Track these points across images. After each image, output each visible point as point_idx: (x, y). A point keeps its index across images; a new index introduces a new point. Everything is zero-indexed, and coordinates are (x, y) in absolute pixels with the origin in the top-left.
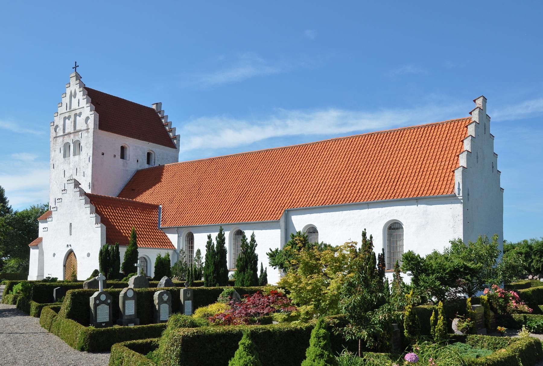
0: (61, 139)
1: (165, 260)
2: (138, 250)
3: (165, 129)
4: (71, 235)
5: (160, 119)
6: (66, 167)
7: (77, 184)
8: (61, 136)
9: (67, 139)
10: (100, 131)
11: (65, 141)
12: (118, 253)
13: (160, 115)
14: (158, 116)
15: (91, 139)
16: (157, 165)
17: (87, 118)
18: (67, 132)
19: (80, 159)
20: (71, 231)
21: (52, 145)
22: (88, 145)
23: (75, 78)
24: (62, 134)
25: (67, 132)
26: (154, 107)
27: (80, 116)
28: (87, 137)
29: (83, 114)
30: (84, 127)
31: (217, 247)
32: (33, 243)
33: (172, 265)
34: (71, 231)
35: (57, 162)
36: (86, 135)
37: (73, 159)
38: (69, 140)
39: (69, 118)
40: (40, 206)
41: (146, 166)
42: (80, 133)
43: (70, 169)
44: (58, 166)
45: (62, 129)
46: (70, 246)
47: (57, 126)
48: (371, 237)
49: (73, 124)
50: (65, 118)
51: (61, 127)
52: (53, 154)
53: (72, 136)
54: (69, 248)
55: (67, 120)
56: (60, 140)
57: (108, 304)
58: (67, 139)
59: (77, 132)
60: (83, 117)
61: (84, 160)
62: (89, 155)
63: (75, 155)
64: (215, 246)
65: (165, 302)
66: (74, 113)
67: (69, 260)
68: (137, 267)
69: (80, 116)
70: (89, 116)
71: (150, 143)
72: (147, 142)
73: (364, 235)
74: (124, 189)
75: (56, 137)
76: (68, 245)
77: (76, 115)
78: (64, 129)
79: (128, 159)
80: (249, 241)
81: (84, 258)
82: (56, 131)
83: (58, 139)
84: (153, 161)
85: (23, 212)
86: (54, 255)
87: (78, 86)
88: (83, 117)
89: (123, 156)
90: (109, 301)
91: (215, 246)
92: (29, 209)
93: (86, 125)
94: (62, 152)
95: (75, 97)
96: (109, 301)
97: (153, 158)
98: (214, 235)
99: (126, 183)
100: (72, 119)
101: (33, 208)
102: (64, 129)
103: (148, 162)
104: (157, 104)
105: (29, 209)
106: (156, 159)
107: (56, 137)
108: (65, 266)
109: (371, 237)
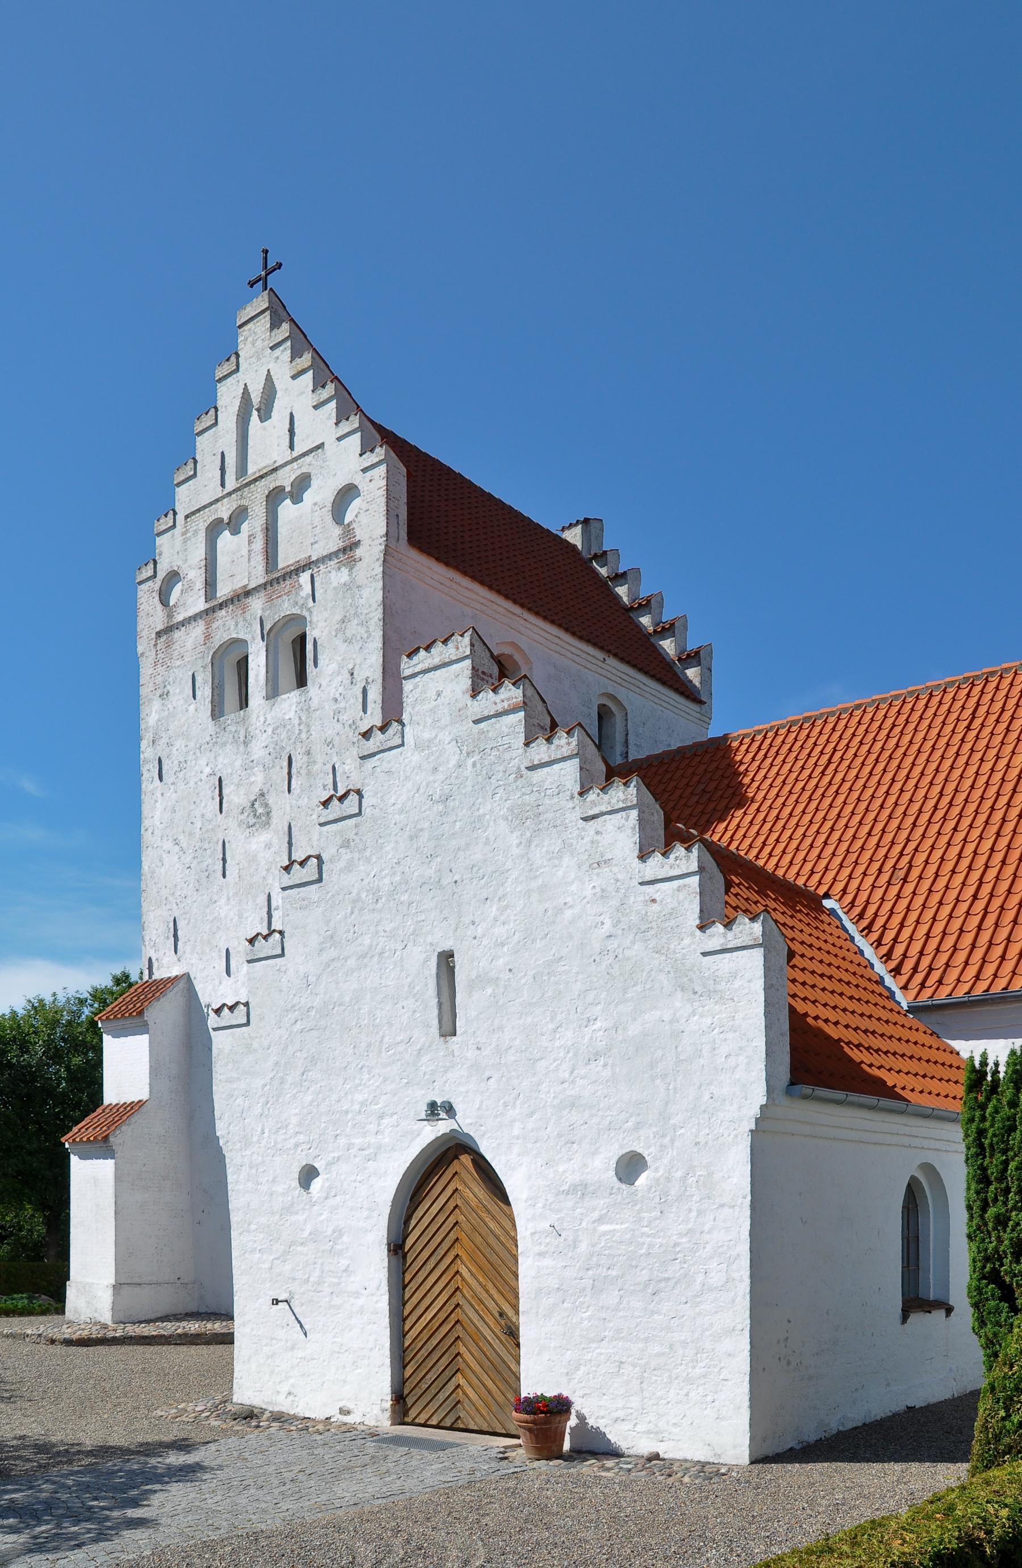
0: (198, 630)
3: (639, 627)
4: (448, 1029)
5: (604, 589)
6: (228, 761)
8: (194, 618)
9: (228, 626)
10: (414, 555)
11: (220, 637)
13: (603, 571)
14: (596, 574)
15: (372, 595)
17: (347, 493)
18: (224, 591)
19: (306, 708)
21: (146, 669)
22: (353, 628)
23: (265, 320)
24: (201, 605)
25: (224, 591)
26: (574, 537)
27: (297, 499)
28: (347, 587)
29: (315, 483)
30: (332, 539)
35: (179, 743)
37: (269, 714)
39: (235, 523)
40: (62, 999)
42: (305, 578)
43: (248, 767)
44: (182, 766)
45: (200, 584)
46: (450, 1110)
47: (174, 577)
49: (259, 544)
50: (214, 530)
51: (195, 575)
52: (152, 714)
53: (257, 605)
54: (443, 1127)
55: (225, 540)
56: (190, 638)
58: (228, 626)
59: (284, 577)
60: (320, 494)
61: (329, 708)
62: (360, 677)
63: (273, 692)
66: (262, 489)
67: (429, 1209)
69: (297, 499)
70: (359, 480)
71: (612, 661)
72: (600, 655)
75: (169, 630)
76: (433, 1106)
77: (275, 497)
78: (210, 584)
81: (582, 1190)
82: (164, 600)
83: (177, 634)
86: (308, 1175)
87: (284, 353)
88: (320, 494)
92: (21, 1012)
93: (337, 531)
94: (205, 692)
95: (265, 413)
97: (619, 737)
100: (255, 523)
101: (38, 1008)
102: (210, 584)
104: (586, 521)
105: (21, 1012)
106: (631, 738)
107: (169, 630)
108: (397, 1248)
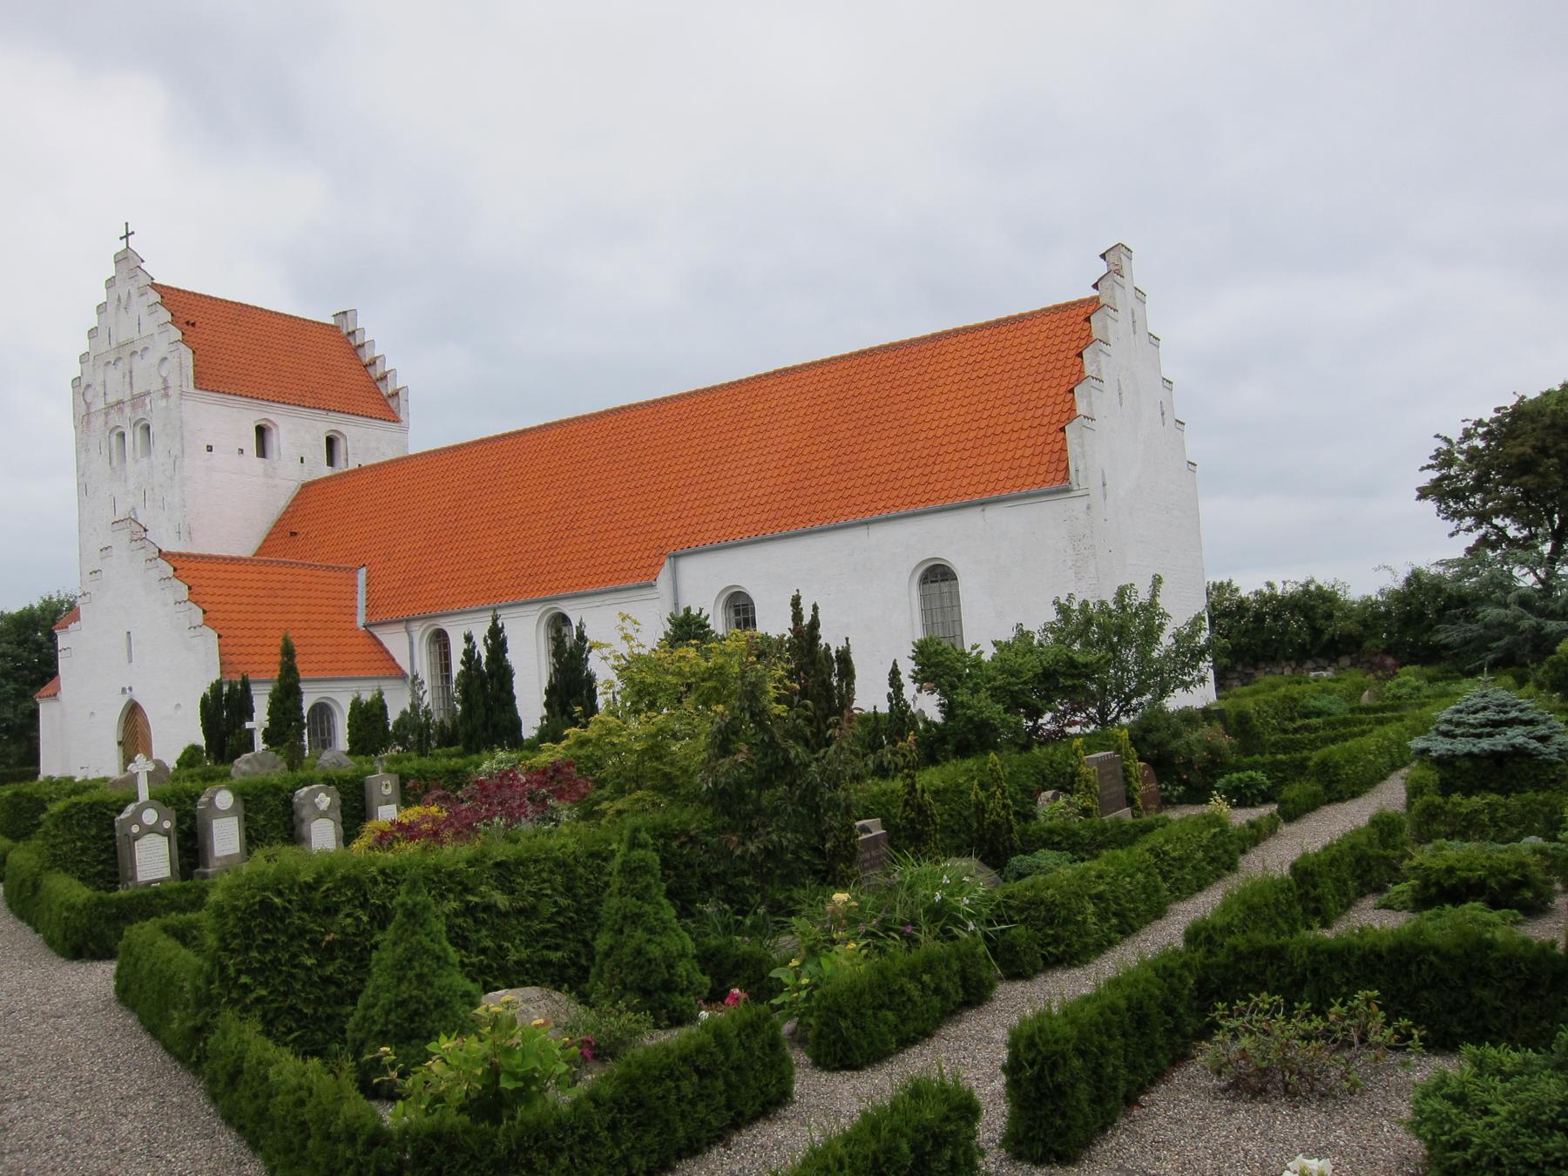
1: (370, 705)
2: (302, 686)
7: (140, 534)
12: (249, 699)
16: (353, 465)
20: (130, 651)
31: (487, 664)
32: (44, 691)
33: (393, 716)
34: (130, 651)
36: (163, 403)
38: (124, 420)
41: (327, 471)
48: (815, 608)
57: (166, 833)
64: (484, 660)
65: (324, 815)
68: (251, 731)
73: (796, 603)
74: (270, 534)
79: (275, 456)
80: (807, 620)
84: (343, 457)
85: (21, 614)
89: (262, 451)
90: (167, 825)
91: (484, 660)
92: (36, 606)
96: (167, 825)
98: (480, 631)
99: (275, 518)
103: (331, 461)
105: (36, 606)
109: (815, 608)
